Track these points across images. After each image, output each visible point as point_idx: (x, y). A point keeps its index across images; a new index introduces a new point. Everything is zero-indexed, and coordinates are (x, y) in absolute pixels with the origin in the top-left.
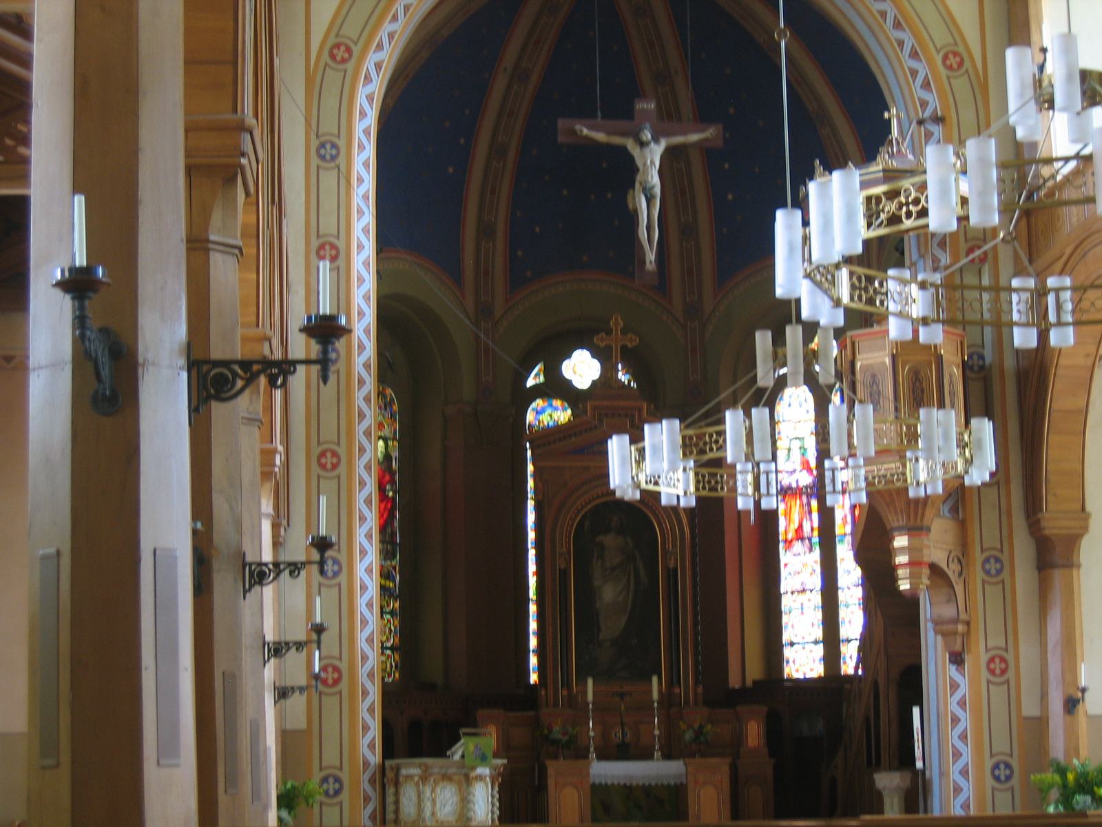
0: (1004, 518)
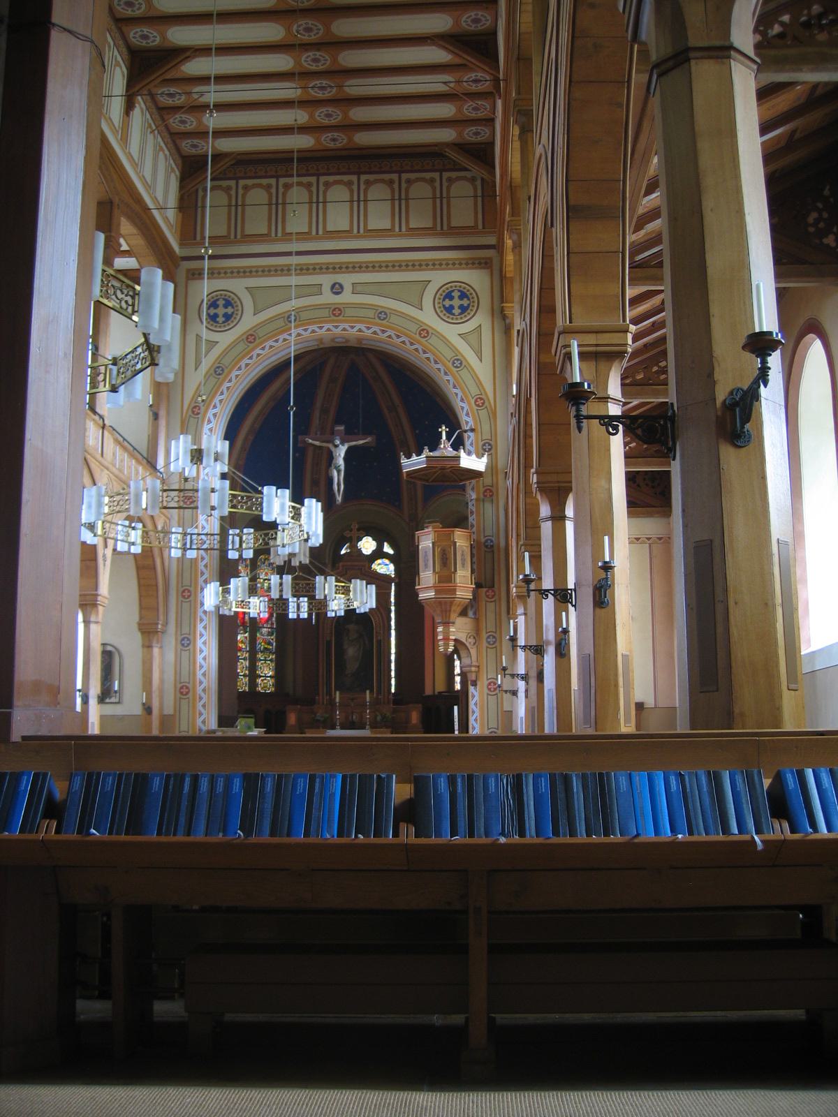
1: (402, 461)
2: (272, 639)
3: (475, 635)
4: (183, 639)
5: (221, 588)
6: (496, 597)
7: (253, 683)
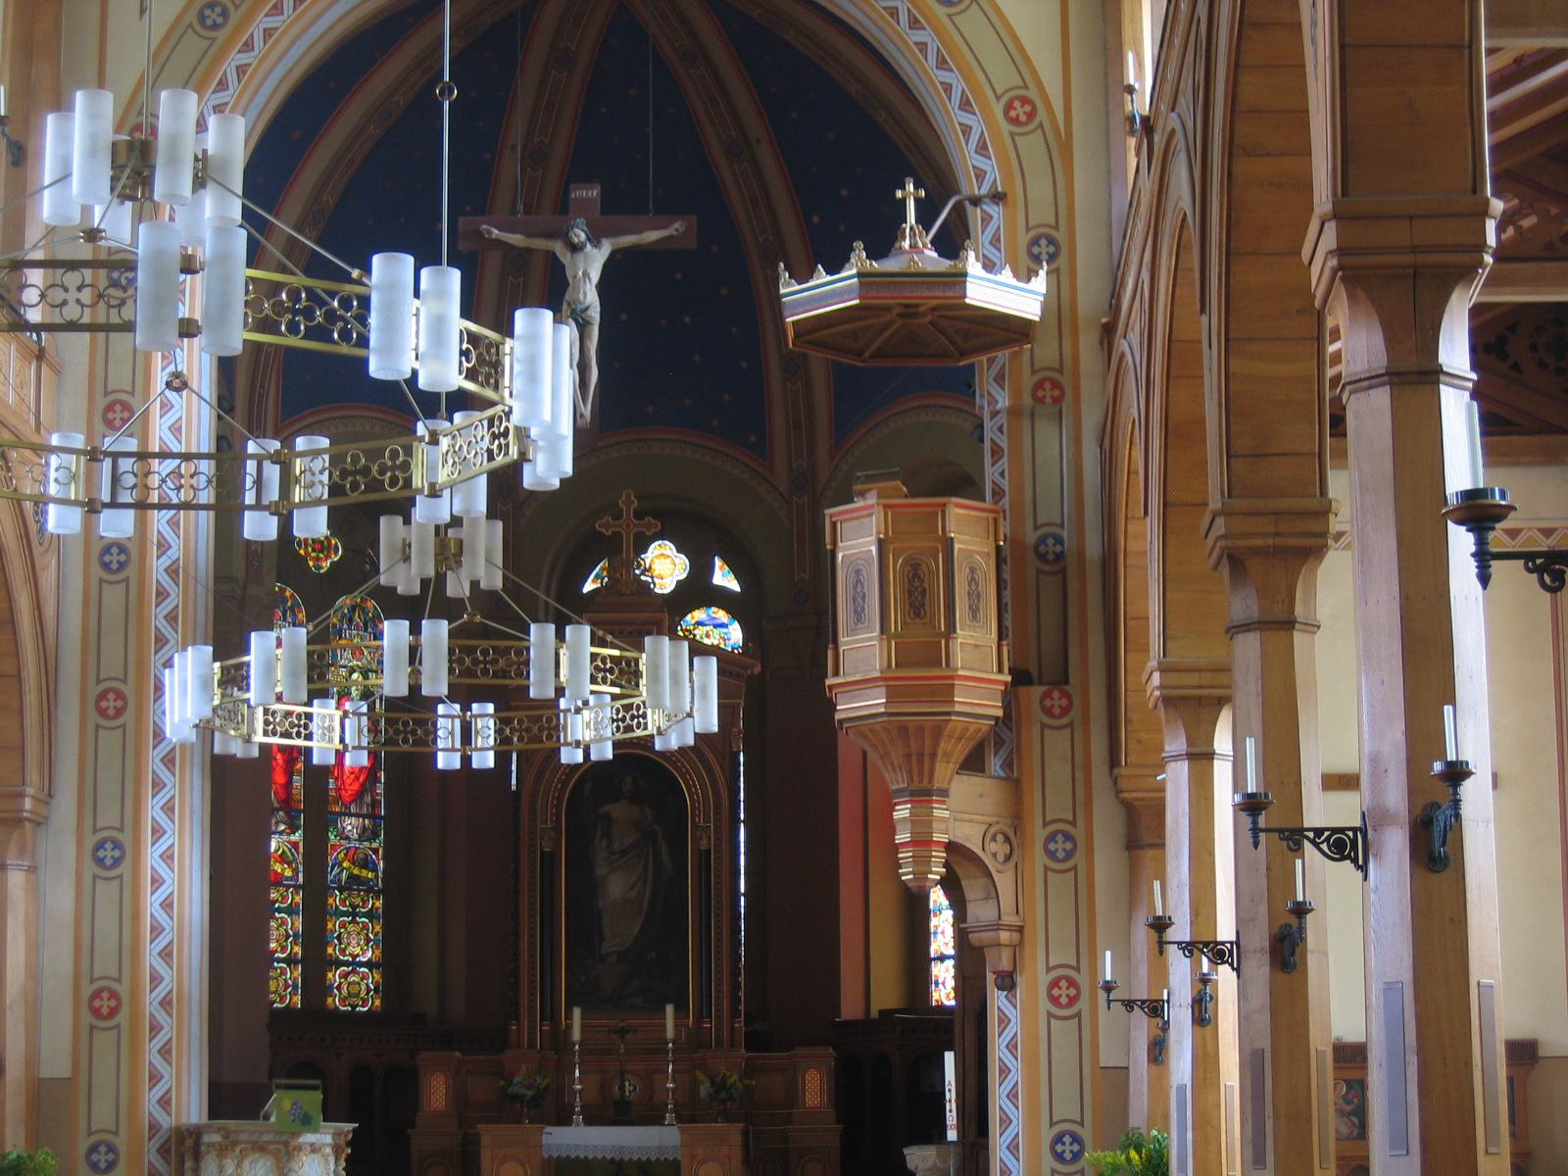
0: (1079, 774)
1: (783, 291)
2: (375, 851)
3: (1011, 833)
4: (100, 846)
5: (217, 665)
6: (1075, 714)
7: (315, 984)
